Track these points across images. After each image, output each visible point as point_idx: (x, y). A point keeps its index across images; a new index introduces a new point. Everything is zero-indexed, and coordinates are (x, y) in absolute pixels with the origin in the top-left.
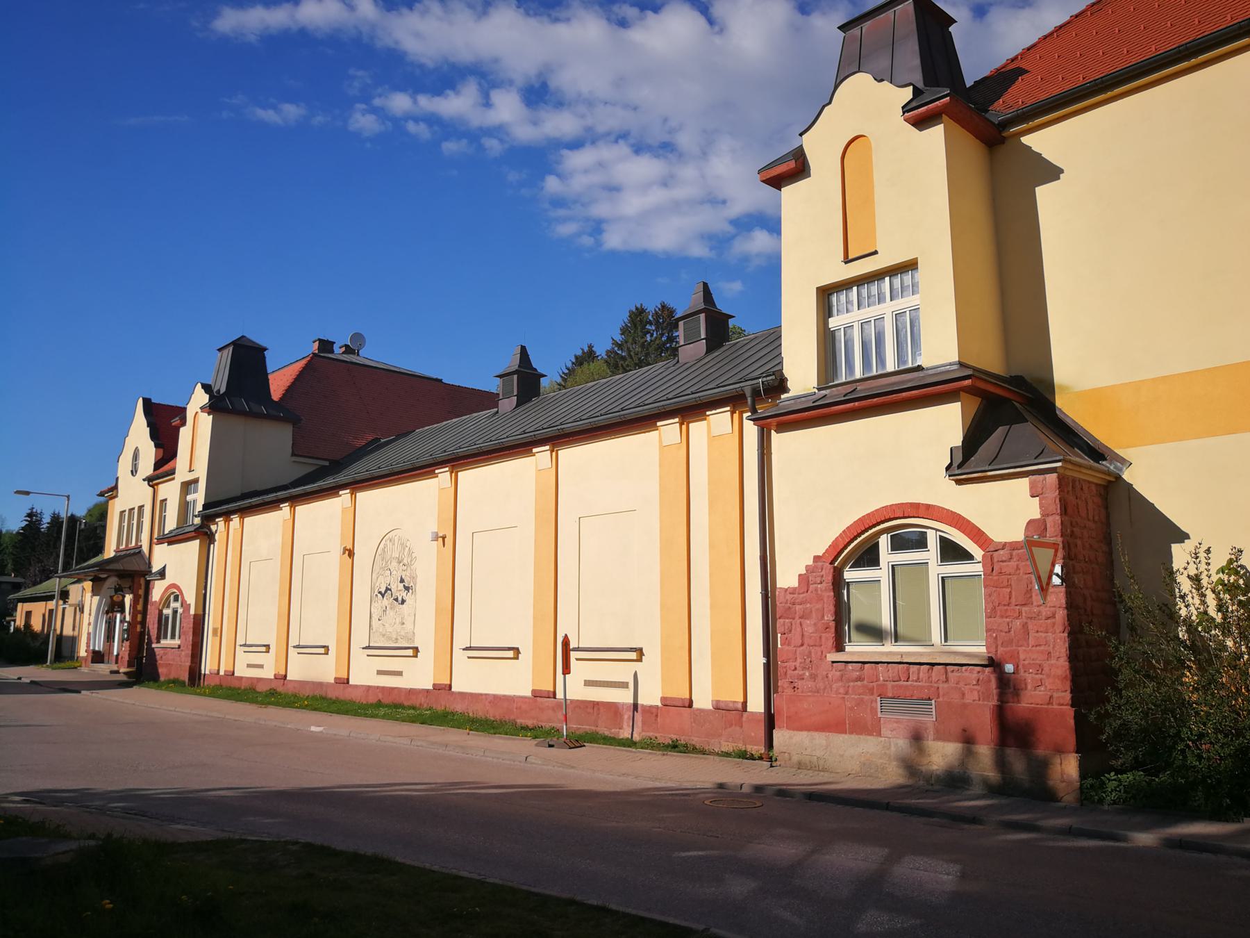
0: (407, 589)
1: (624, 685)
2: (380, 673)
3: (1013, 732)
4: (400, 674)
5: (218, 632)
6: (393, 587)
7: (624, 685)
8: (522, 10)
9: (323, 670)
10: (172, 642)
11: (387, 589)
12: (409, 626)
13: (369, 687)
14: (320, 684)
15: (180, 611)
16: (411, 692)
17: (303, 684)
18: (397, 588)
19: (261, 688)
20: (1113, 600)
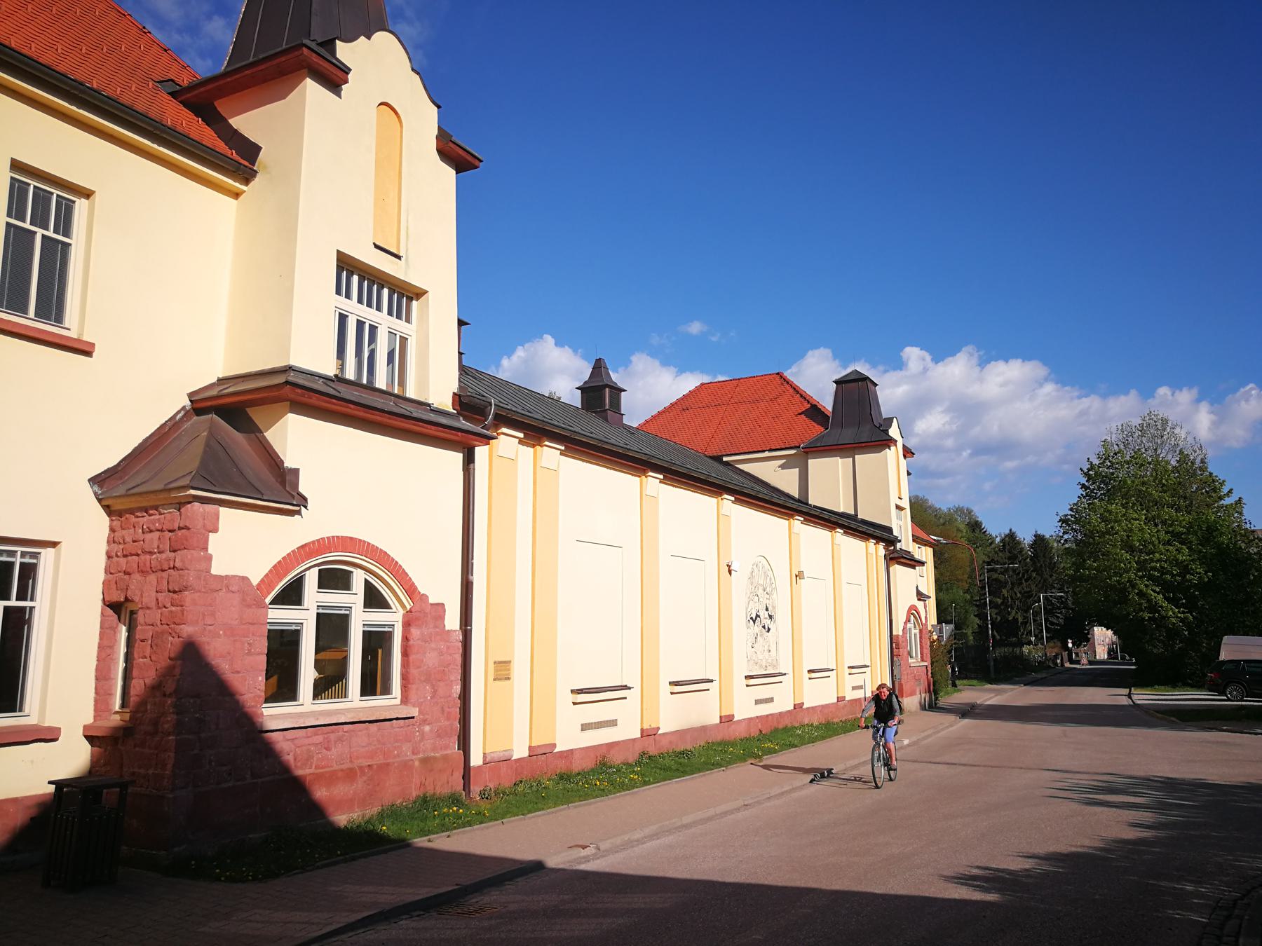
0: (771, 617)
1: (860, 687)
2: (758, 702)
3: (1083, 486)
4: (613, 723)
5: (502, 670)
6: (761, 614)
7: (860, 687)
8: (837, 362)
9: (700, 712)
10: (331, 708)
11: (757, 616)
12: (773, 652)
13: (750, 719)
14: (704, 729)
15: (361, 620)
16: (781, 715)
17: (681, 734)
18: (764, 614)
19: (617, 758)
20: (985, 879)
